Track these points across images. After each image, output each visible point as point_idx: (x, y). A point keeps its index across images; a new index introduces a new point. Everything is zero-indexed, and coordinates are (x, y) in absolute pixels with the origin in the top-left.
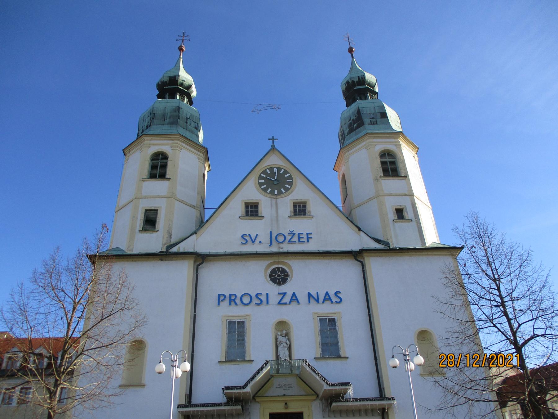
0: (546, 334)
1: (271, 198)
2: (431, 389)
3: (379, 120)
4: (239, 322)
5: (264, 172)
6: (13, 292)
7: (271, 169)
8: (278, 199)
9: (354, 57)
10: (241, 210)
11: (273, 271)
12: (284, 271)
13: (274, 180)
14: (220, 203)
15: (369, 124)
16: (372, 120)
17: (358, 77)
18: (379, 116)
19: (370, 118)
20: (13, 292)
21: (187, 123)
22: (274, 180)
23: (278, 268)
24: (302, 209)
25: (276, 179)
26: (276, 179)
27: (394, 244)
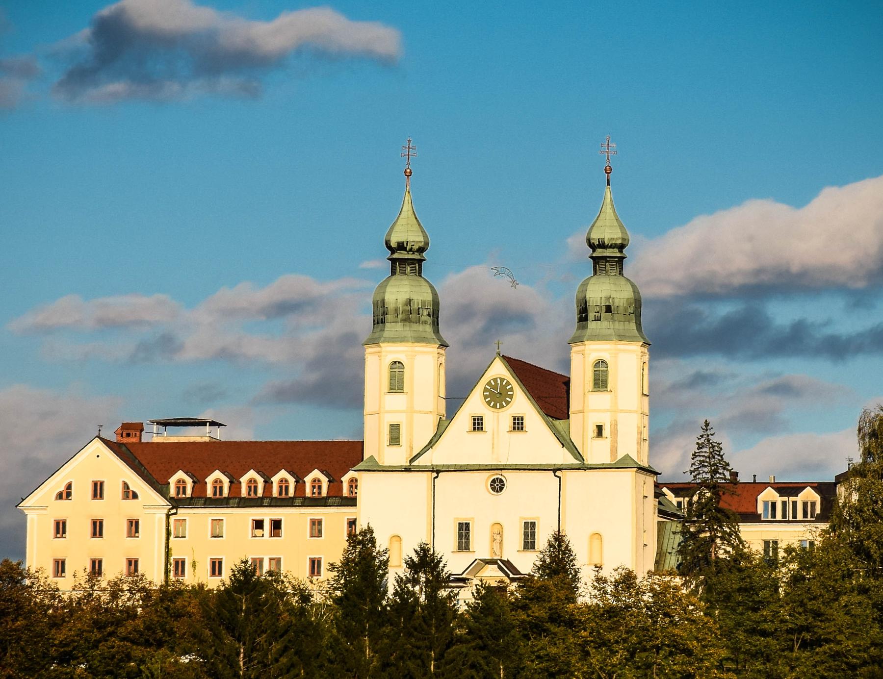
0: (756, 482)
1: (493, 412)
2: (712, 428)
3: (603, 314)
4: (466, 523)
5: (489, 383)
6: (460, 654)
7: (495, 380)
8: (500, 413)
9: (588, 247)
10: (469, 424)
11: (494, 481)
12: (501, 481)
13: (497, 392)
14: (466, 568)
15: (593, 321)
16: (597, 314)
17: (599, 239)
18: (604, 309)
19: (595, 312)
20: (460, 654)
21: (419, 314)
22: (497, 392)
23: (497, 479)
24: (520, 421)
25: (498, 391)
26: (498, 391)
27: (589, 460)
